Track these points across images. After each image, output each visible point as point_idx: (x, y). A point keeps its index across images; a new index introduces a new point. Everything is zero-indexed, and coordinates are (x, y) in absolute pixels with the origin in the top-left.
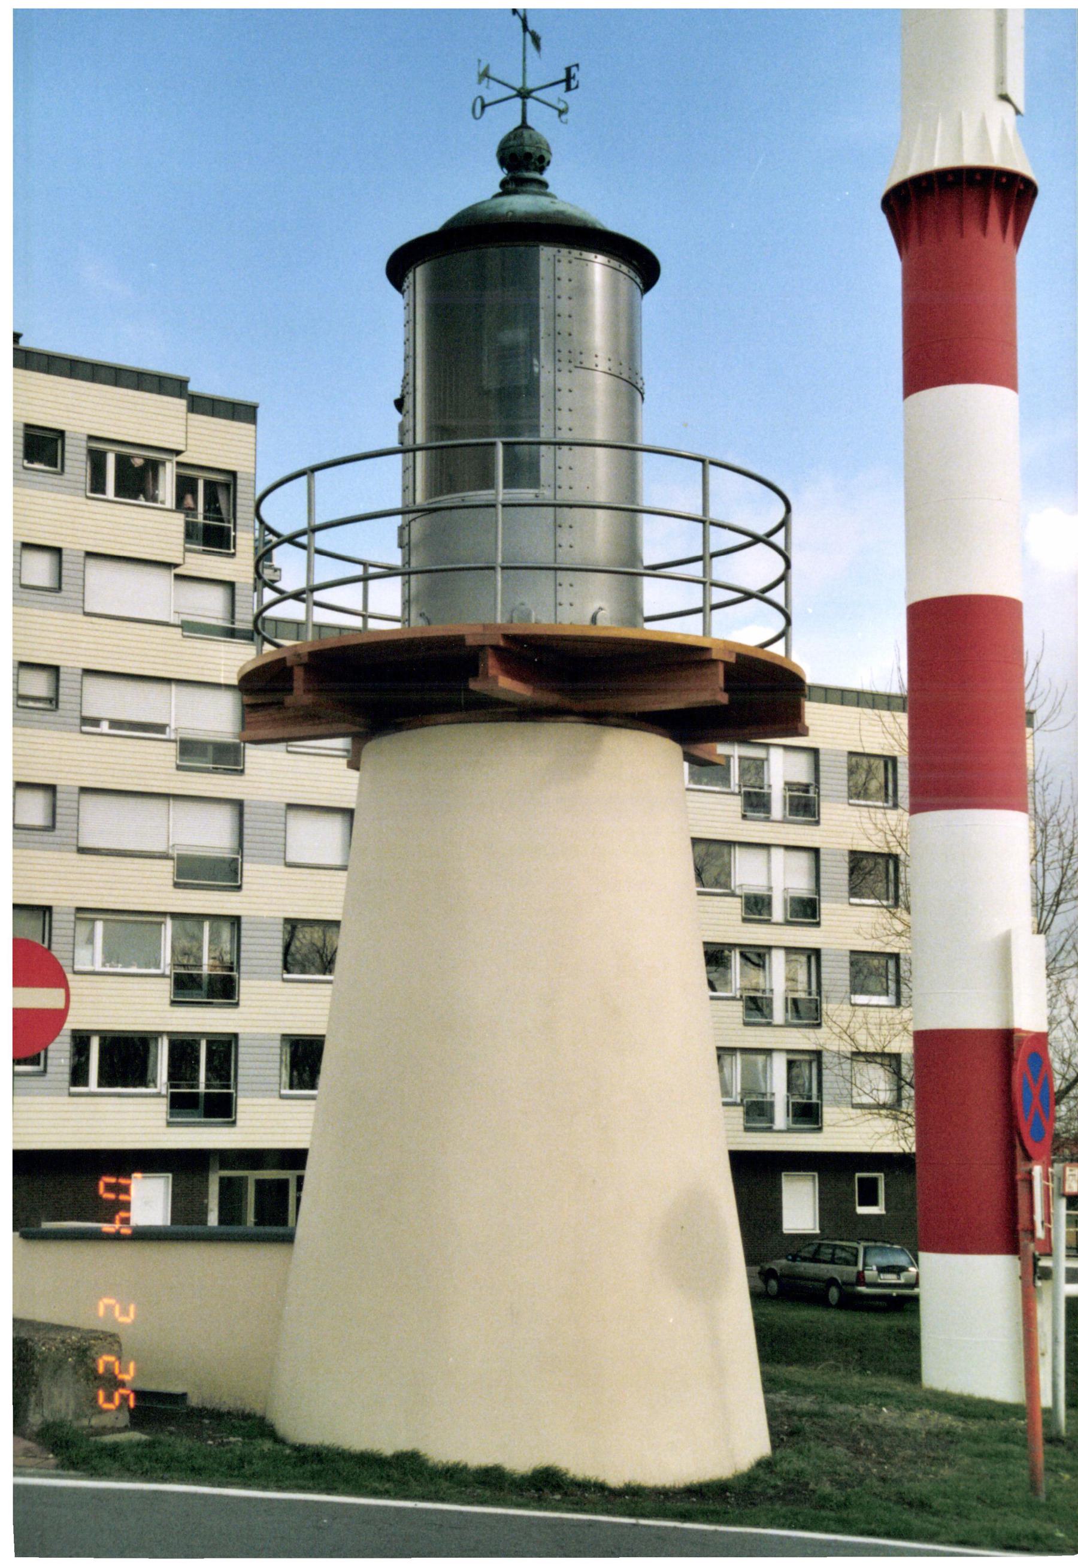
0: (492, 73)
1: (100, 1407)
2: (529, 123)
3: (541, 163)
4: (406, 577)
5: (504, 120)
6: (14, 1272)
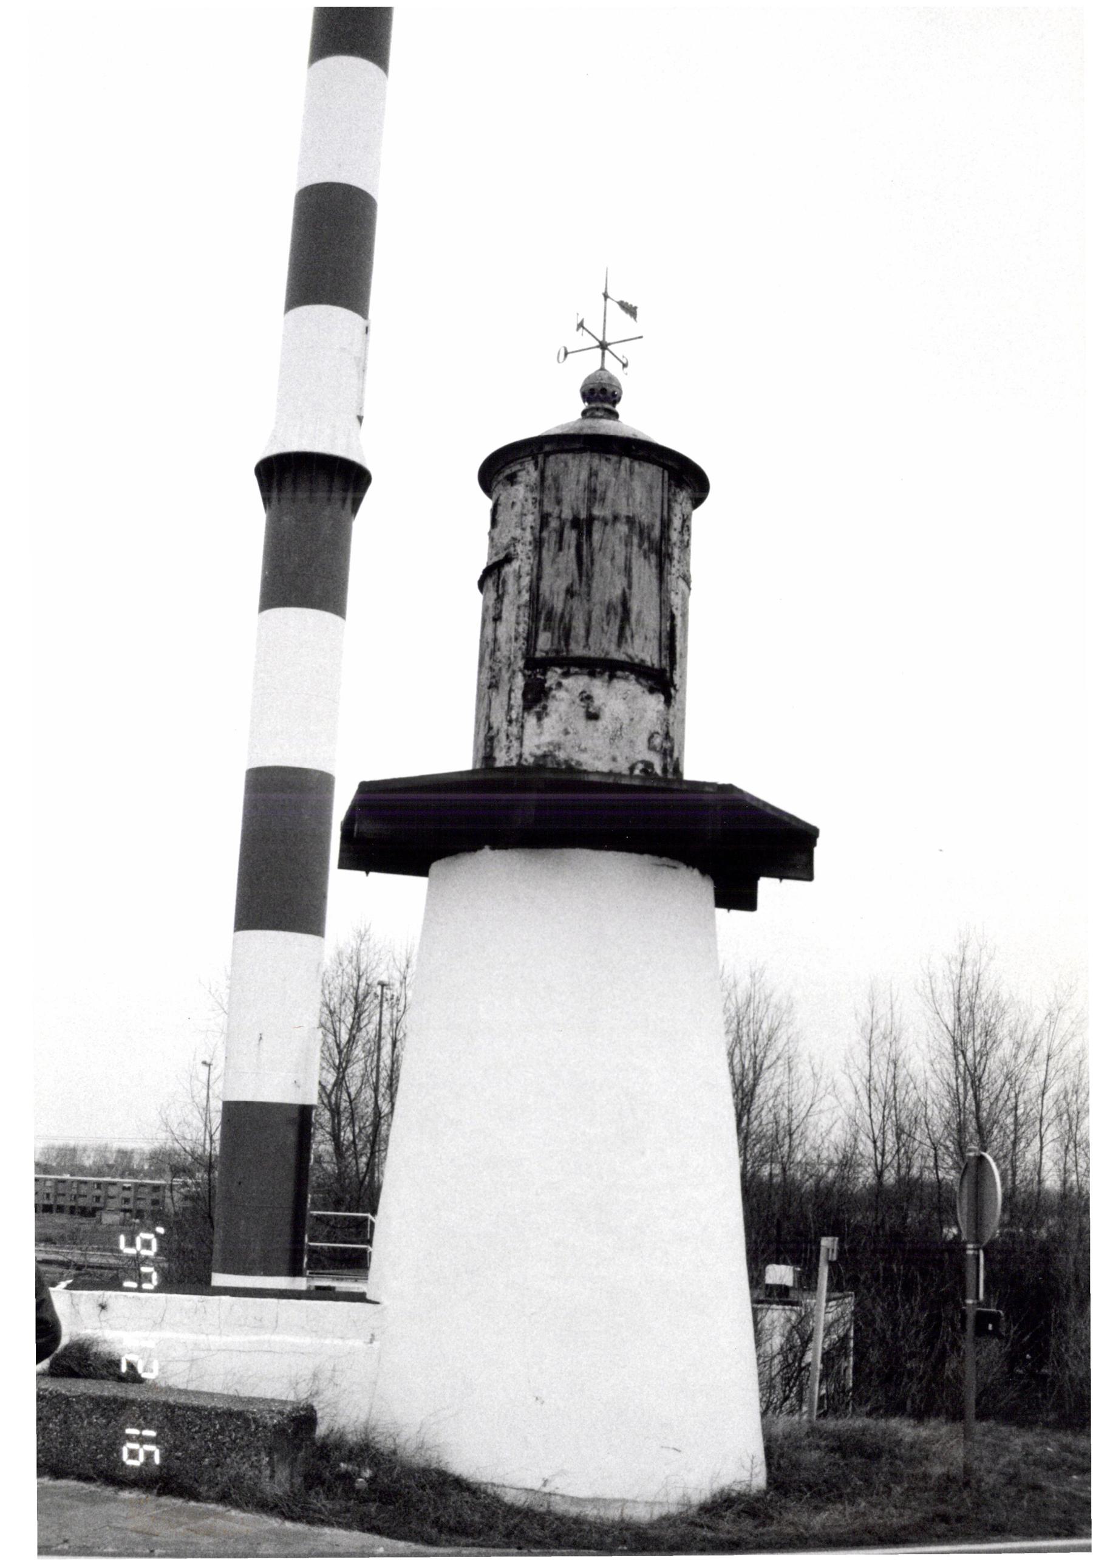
0: (585, 325)
1: (142, 1464)
2: (606, 367)
3: (615, 399)
4: (595, 732)
5: (587, 365)
6: (40, 1511)
